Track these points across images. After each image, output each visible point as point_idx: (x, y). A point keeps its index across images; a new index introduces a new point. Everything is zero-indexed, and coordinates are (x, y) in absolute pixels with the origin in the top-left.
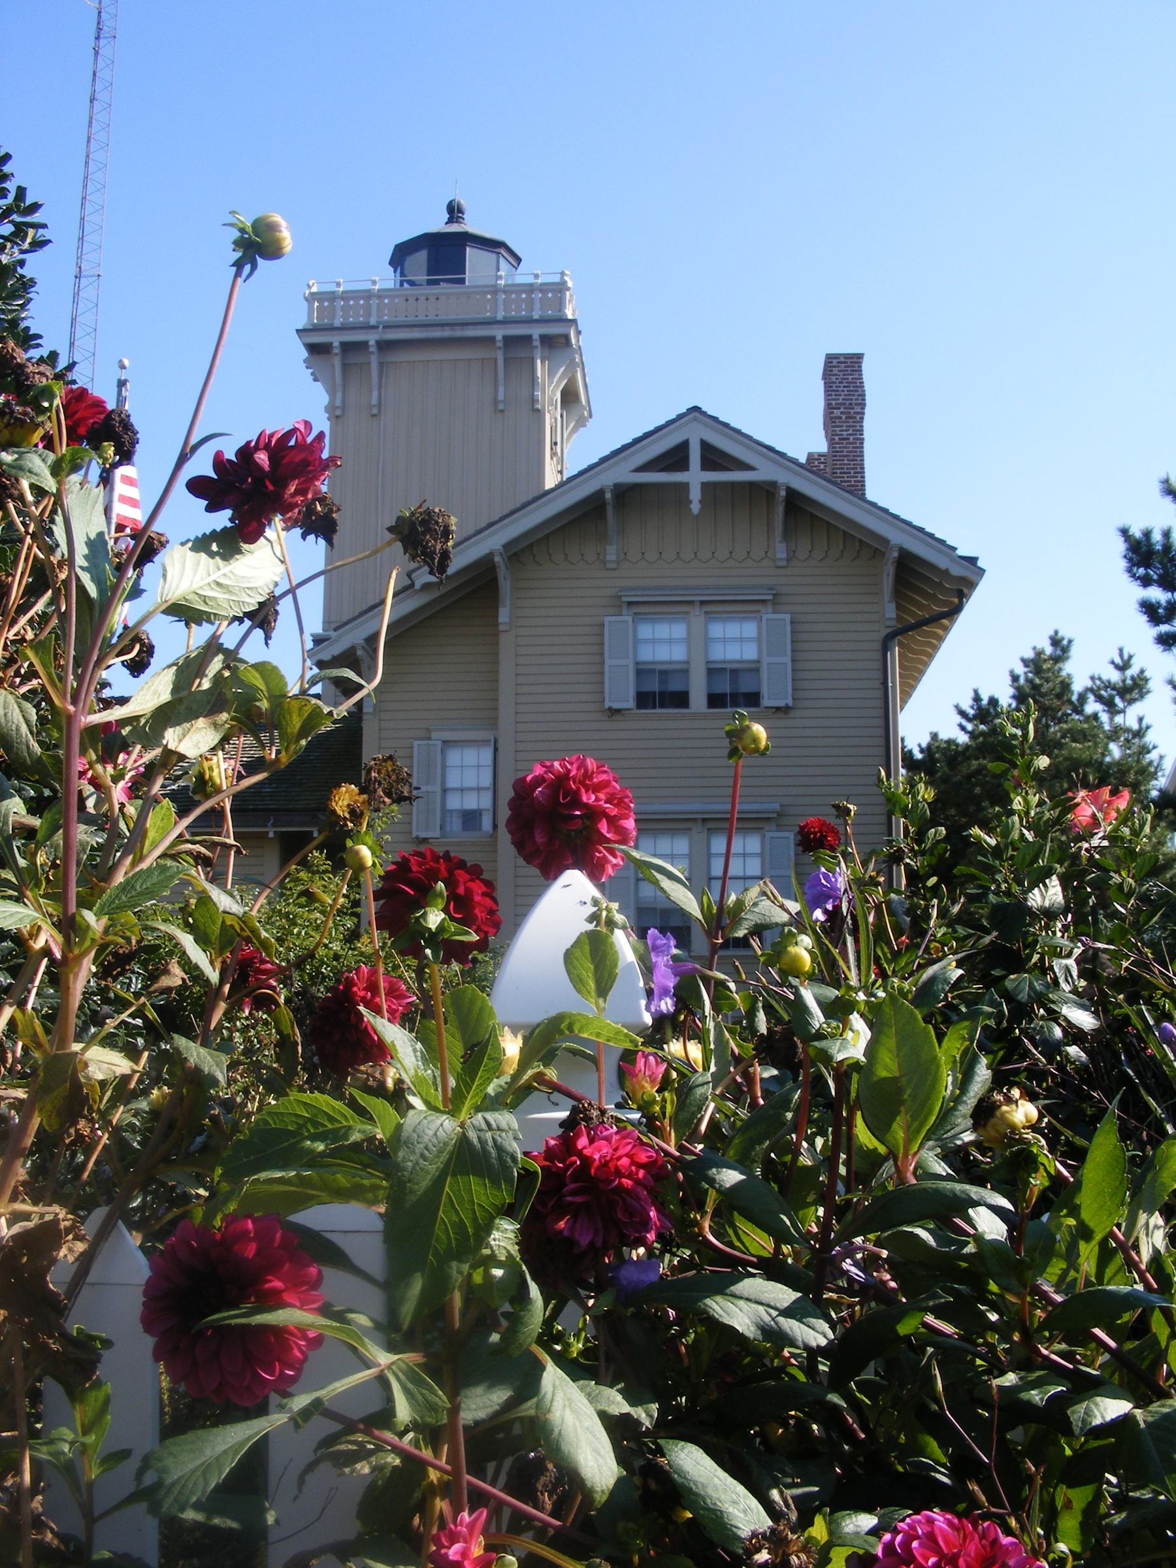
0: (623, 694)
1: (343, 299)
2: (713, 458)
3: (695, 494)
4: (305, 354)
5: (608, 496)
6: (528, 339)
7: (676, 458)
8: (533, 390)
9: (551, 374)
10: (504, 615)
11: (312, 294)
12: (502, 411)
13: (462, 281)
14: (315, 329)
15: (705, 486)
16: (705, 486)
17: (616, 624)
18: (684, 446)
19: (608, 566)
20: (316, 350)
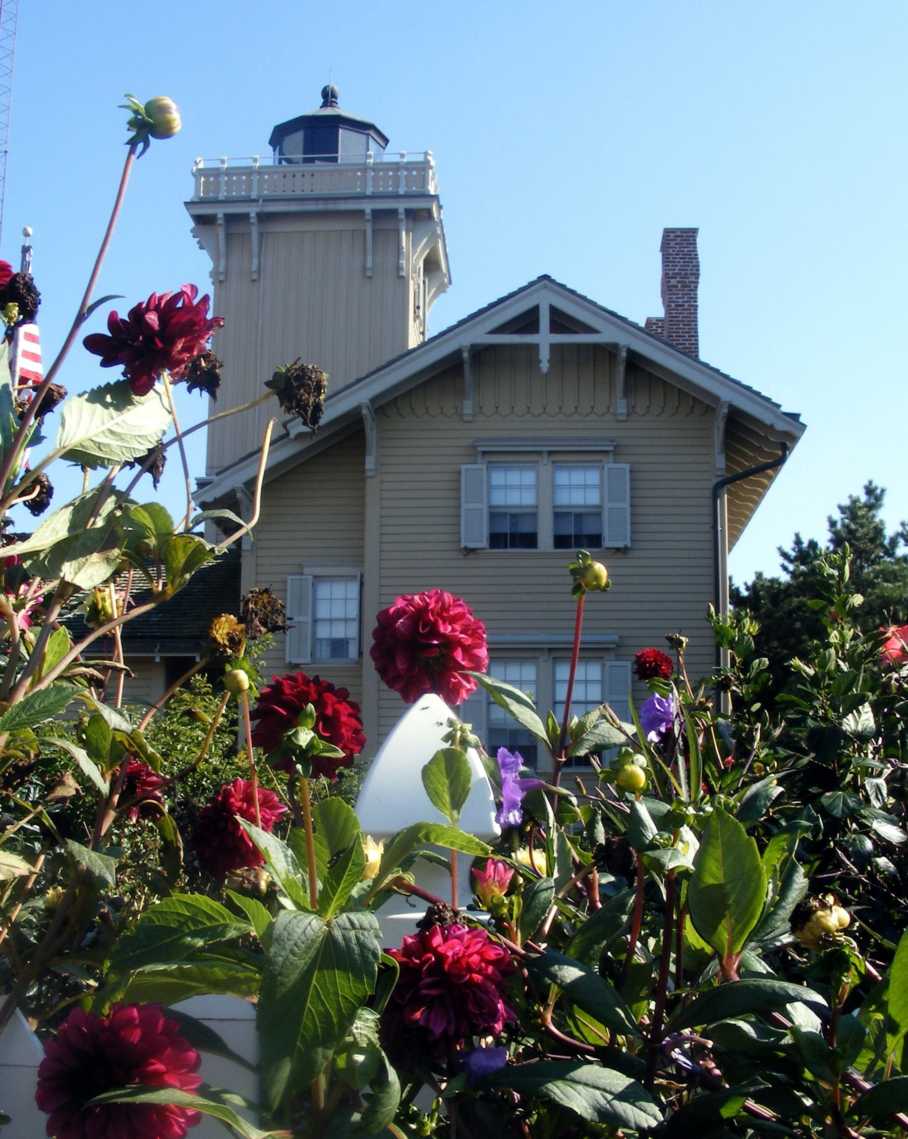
0: (476, 534)
1: (227, 175)
2: (562, 322)
3: (544, 354)
4: (192, 224)
5: (466, 355)
6: (394, 212)
7: (527, 322)
8: (399, 259)
9: (415, 245)
10: (370, 463)
11: (198, 170)
12: (370, 278)
13: (335, 160)
14: (201, 202)
15: (553, 347)
16: (553, 347)
17: (472, 472)
18: (534, 311)
19: (465, 419)
20: (202, 221)
